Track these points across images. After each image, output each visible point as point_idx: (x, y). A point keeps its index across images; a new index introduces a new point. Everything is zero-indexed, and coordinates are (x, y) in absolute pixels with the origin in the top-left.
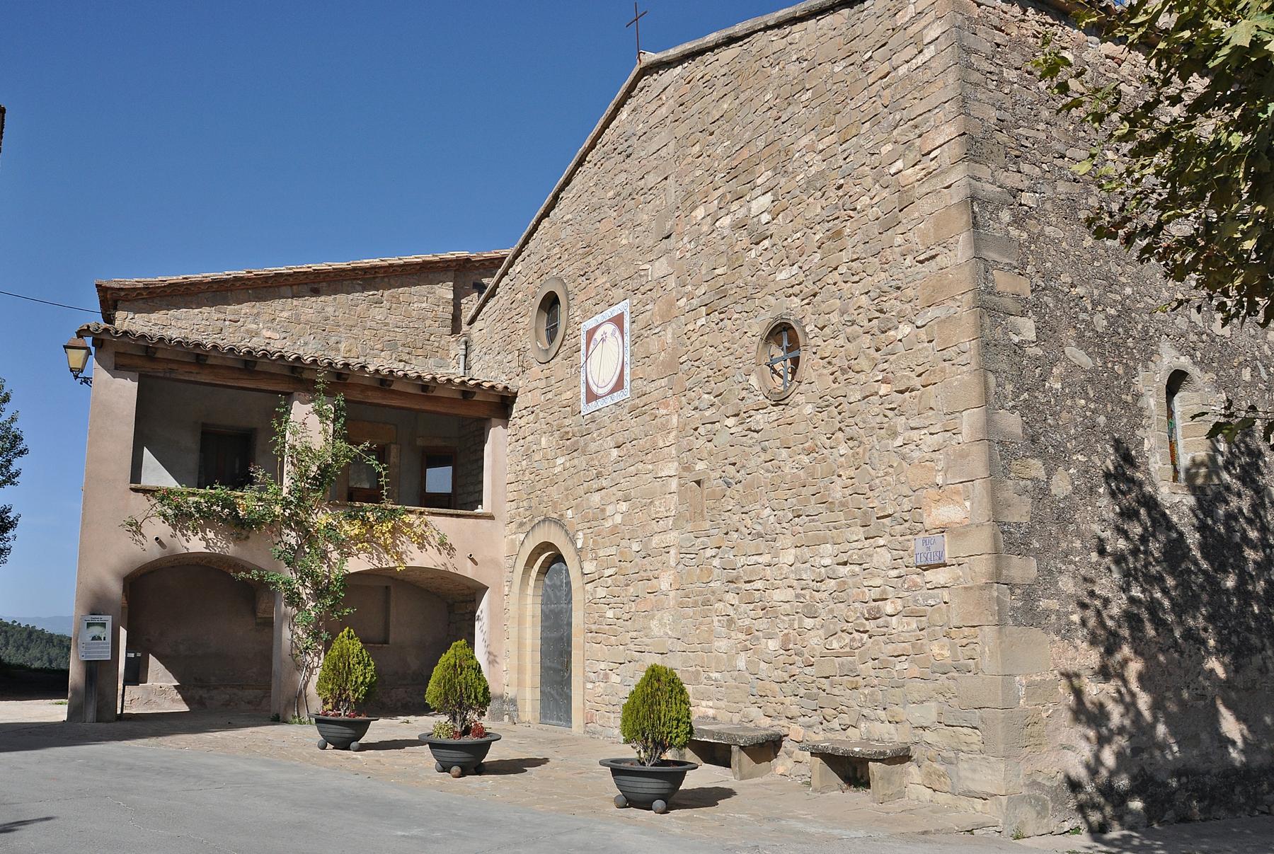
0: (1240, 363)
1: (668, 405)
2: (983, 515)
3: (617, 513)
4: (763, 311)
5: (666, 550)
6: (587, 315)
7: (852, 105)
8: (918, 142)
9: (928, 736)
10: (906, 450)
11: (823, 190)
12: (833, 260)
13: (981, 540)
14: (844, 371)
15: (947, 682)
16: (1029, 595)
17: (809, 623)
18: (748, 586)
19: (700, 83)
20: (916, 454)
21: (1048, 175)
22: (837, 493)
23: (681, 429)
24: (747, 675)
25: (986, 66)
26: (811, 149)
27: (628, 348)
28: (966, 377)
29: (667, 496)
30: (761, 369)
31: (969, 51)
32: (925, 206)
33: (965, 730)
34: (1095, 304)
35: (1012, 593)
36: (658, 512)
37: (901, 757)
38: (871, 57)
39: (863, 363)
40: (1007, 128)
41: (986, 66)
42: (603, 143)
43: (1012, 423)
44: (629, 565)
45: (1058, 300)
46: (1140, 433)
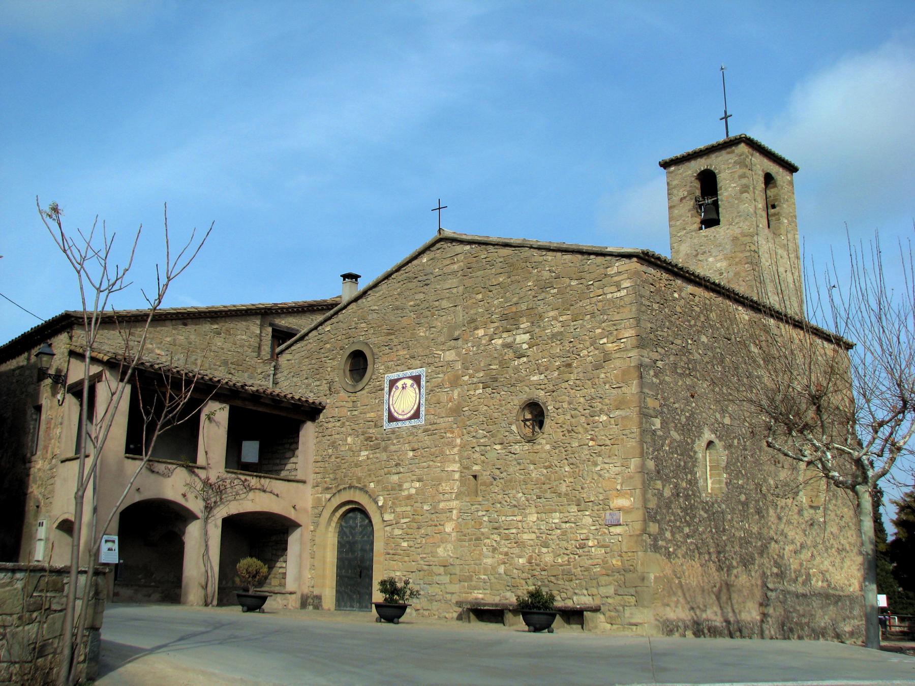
0: (734, 437)
1: (454, 432)
2: (639, 504)
3: (411, 488)
4: (521, 394)
5: (450, 510)
6: (388, 370)
7: (581, 304)
8: (615, 332)
9: (610, 600)
10: (602, 472)
11: (562, 341)
12: (566, 377)
13: (638, 515)
14: (569, 432)
15: (619, 577)
16: (656, 540)
17: (544, 550)
18: (506, 531)
19: (484, 261)
20: (607, 475)
21: (667, 353)
22: (563, 488)
23: (463, 447)
24: (505, 576)
25: (647, 303)
26: (555, 318)
27: (424, 396)
28: (634, 444)
29: (451, 481)
30: (519, 423)
31: (642, 296)
32: (618, 363)
33: (628, 597)
34: (682, 411)
35: (650, 538)
36: (445, 490)
37: (597, 610)
38: (592, 284)
39: (581, 430)
40: (654, 332)
41: (647, 303)
42: (406, 271)
43: (651, 464)
44: (420, 517)
45: (669, 410)
46: (696, 469)
